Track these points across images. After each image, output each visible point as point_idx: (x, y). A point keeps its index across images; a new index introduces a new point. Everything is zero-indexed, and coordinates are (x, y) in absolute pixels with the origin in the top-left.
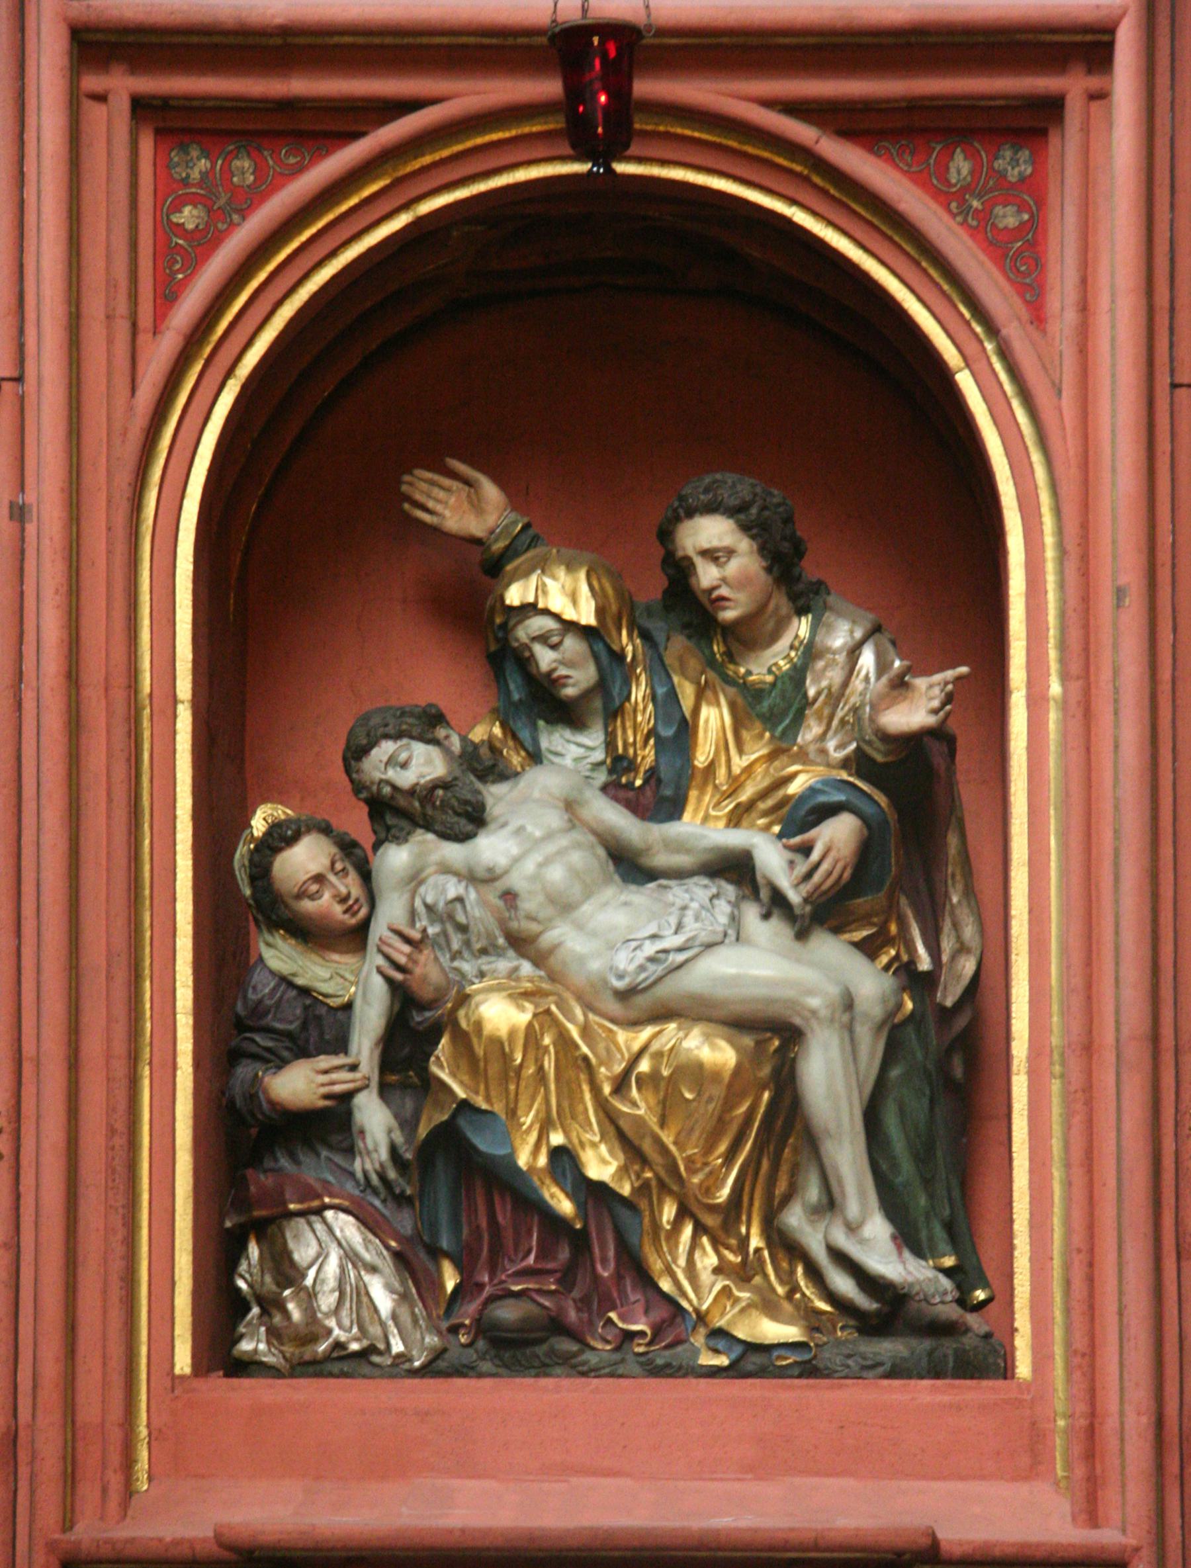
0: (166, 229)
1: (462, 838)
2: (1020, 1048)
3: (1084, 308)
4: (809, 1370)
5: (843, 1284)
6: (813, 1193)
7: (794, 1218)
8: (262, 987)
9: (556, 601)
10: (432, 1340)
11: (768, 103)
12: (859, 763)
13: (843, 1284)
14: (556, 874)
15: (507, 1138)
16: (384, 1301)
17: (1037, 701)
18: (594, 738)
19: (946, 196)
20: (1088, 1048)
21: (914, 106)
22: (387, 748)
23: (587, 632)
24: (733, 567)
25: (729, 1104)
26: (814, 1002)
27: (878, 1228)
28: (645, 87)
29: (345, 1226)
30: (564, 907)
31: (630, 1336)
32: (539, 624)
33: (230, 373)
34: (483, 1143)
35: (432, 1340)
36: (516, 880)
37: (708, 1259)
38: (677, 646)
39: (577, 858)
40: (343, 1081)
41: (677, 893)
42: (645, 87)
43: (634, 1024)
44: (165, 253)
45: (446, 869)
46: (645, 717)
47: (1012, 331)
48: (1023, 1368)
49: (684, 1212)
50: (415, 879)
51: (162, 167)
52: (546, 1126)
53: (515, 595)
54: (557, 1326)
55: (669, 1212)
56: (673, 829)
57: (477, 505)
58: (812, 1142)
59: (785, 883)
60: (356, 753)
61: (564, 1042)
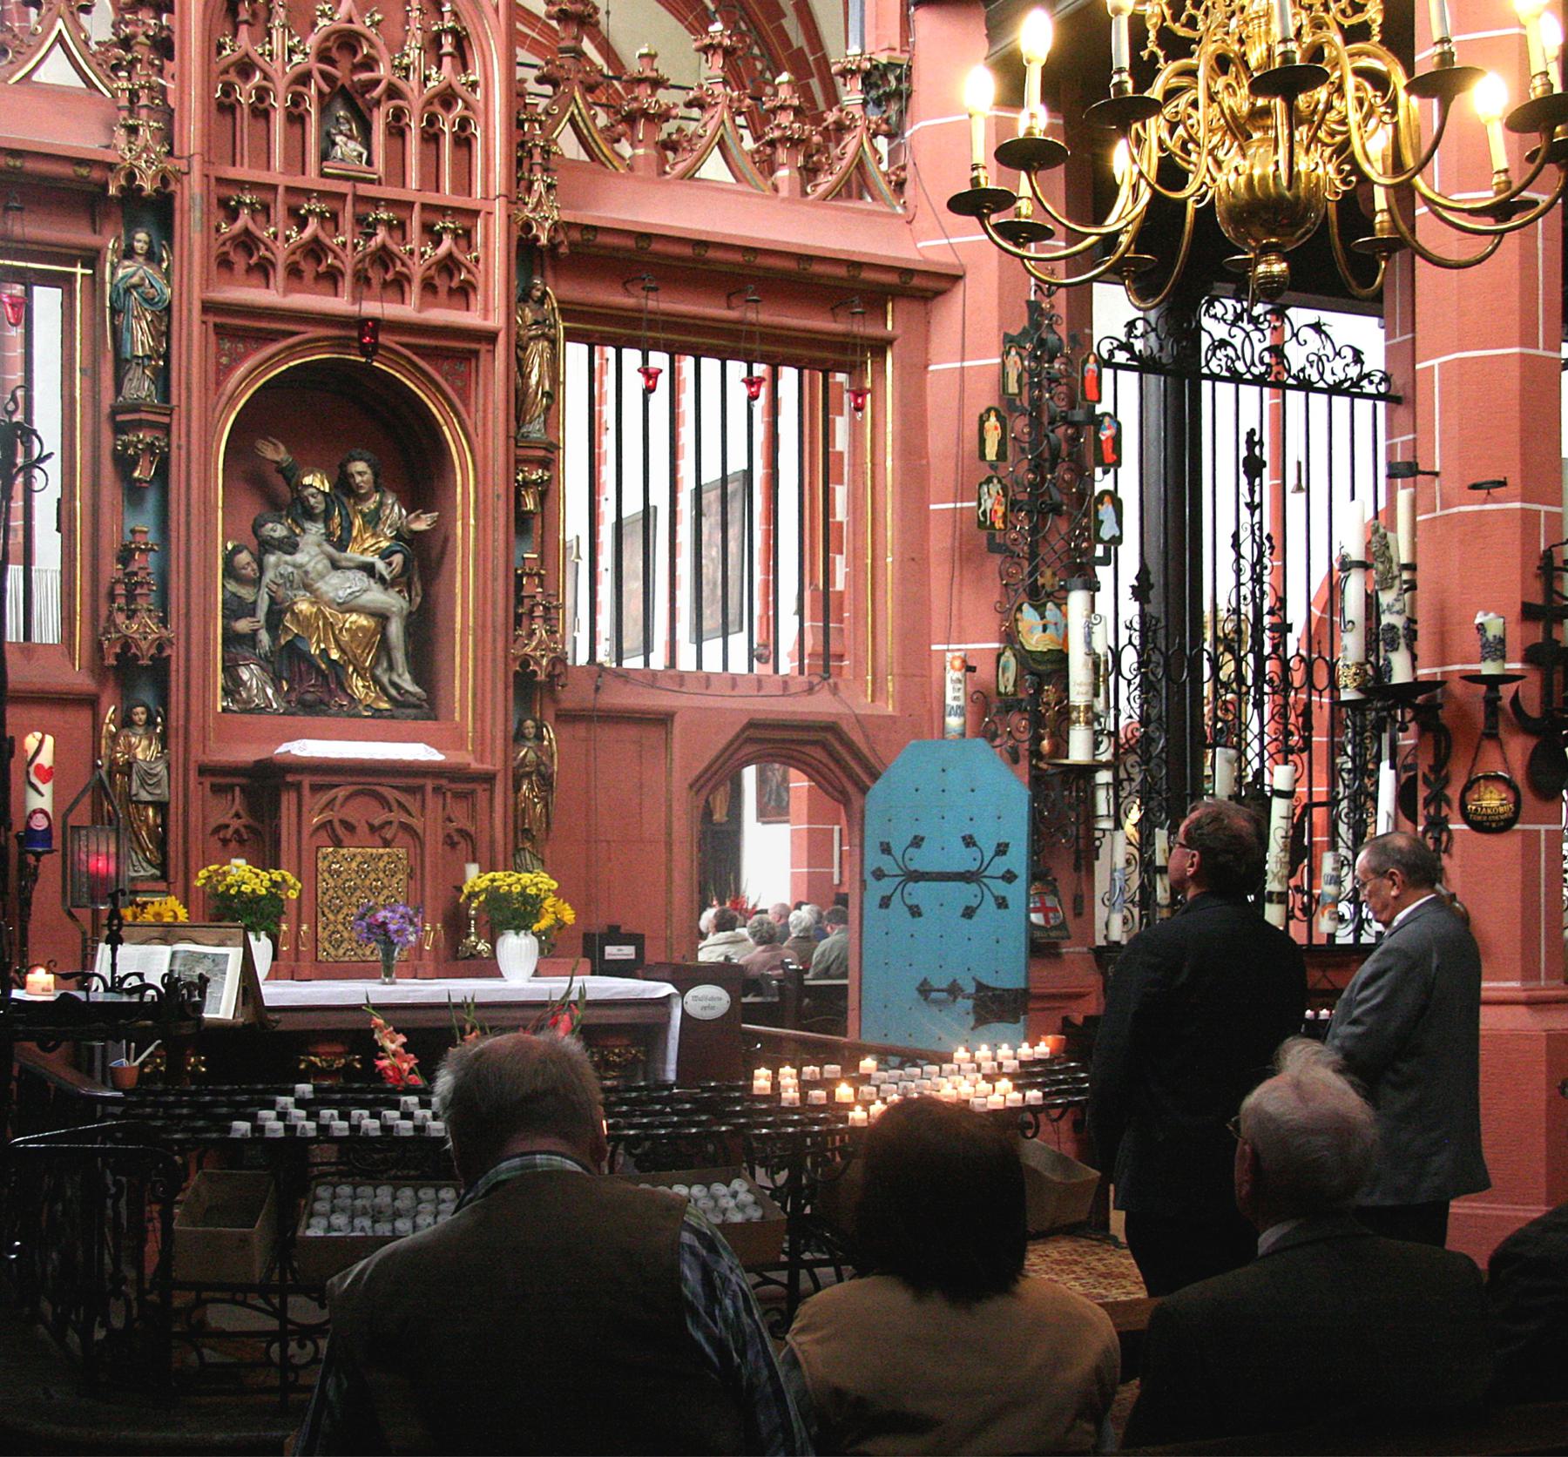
0: (218, 363)
1: (291, 554)
4: (393, 717)
5: (393, 692)
6: (385, 665)
7: (379, 672)
9: (317, 484)
12: (396, 538)
14: (320, 567)
15: (309, 646)
16: (270, 692)
19: (438, 370)
22: (270, 525)
24: (366, 477)
27: (407, 676)
28: (382, 339)
30: (322, 576)
32: (312, 490)
34: (300, 645)
36: (309, 568)
37: (360, 683)
40: (257, 626)
41: (350, 574)
44: (218, 371)
46: (337, 520)
47: (465, 416)
48: (457, 717)
49: (355, 670)
50: (277, 565)
51: (218, 344)
52: (318, 643)
54: (321, 702)
55: (351, 669)
59: (385, 573)
61: (325, 618)
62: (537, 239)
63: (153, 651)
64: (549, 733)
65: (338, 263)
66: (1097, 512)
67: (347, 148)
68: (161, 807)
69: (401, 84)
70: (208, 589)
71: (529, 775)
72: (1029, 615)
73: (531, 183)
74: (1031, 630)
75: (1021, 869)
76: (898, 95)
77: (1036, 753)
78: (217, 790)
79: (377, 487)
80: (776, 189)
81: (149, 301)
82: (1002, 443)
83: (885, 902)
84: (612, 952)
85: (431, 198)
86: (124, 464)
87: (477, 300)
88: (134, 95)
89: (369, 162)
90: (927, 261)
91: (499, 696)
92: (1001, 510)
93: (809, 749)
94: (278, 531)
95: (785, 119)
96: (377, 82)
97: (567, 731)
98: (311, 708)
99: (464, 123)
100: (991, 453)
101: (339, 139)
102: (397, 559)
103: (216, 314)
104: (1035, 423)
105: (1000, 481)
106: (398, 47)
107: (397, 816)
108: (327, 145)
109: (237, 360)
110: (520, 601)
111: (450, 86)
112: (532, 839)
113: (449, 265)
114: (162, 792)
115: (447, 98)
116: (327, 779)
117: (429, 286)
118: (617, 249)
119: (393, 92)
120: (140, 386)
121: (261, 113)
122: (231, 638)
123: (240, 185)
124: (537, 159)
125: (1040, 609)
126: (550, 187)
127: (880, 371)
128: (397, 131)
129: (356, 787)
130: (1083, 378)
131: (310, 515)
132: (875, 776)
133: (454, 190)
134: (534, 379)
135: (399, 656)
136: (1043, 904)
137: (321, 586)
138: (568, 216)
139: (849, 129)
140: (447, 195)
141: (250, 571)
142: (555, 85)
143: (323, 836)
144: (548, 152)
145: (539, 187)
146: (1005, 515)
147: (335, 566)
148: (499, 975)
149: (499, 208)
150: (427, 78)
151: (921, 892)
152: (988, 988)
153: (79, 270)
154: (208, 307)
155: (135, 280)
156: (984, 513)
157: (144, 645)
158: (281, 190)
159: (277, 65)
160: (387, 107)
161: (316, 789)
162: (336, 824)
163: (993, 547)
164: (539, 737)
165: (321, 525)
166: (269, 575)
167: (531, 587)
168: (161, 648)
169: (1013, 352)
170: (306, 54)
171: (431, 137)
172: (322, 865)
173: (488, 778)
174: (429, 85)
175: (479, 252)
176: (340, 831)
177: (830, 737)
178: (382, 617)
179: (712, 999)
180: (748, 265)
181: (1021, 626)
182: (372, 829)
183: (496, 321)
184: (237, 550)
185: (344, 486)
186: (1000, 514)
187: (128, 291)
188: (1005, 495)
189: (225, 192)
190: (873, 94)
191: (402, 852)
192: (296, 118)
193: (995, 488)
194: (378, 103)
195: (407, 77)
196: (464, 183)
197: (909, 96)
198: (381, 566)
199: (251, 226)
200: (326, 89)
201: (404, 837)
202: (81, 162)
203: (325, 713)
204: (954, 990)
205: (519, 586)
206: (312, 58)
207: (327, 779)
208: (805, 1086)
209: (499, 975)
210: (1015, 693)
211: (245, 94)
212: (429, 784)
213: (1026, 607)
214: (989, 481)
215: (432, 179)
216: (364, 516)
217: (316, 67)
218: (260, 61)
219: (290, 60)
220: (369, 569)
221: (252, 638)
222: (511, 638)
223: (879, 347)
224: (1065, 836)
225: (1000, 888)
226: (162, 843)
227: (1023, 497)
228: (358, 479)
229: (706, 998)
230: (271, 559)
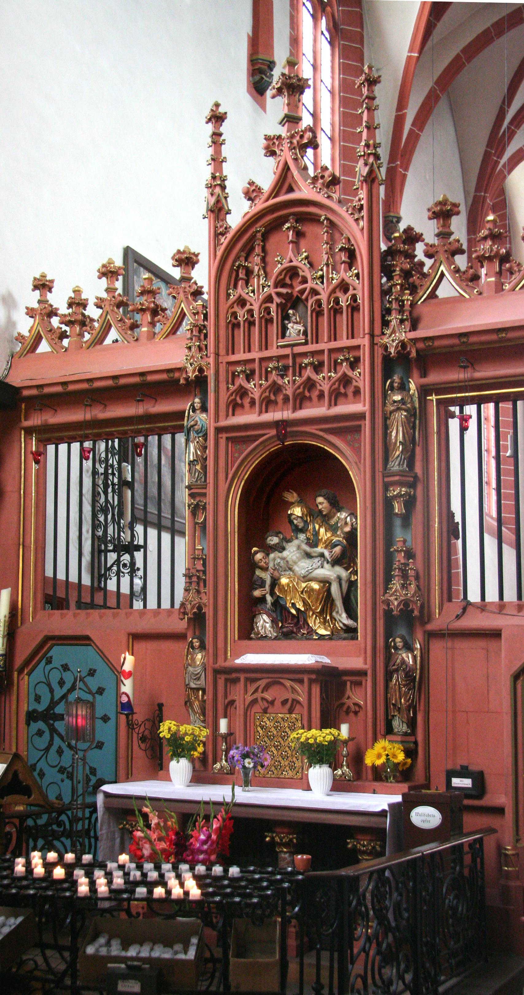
1: (281, 552)
4: (331, 639)
8: (255, 578)
10: (275, 634)
11: (317, 430)
14: (294, 558)
21: (340, 428)
22: (270, 538)
23: (300, 517)
24: (324, 505)
25: (318, 595)
26: (332, 578)
27: (344, 615)
28: (289, 429)
29: (265, 617)
30: (295, 563)
31: (304, 634)
33: (243, 479)
35: (275, 634)
36: (288, 559)
39: (298, 555)
40: (264, 593)
42: (289, 429)
43: (306, 582)
45: (279, 557)
50: (274, 559)
54: (292, 632)
55: (311, 613)
56: (315, 549)
57: (293, 497)
58: (333, 600)
62: (409, 353)
84: (467, 783)
98: (287, 635)
101: (289, 326)
103: (226, 433)
114: (202, 682)
116: (254, 675)
118: (452, 346)
129: (270, 680)
147: (309, 556)
148: (309, 789)
170: (269, 286)
173: (362, 673)
174: (333, 282)
178: (326, 583)
179: (429, 815)
180: (502, 340)
195: (322, 283)
198: (327, 553)
203: (295, 638)
206: (271, 287)
207: (254, 675)
208: (49, 866)
209: (309, 789)
211: (242, 315)
217: (273, 291)
218: (246, 297)
219: (263, 290)
221: (263, 599)
228: (320, 507)
229: (423, 815)
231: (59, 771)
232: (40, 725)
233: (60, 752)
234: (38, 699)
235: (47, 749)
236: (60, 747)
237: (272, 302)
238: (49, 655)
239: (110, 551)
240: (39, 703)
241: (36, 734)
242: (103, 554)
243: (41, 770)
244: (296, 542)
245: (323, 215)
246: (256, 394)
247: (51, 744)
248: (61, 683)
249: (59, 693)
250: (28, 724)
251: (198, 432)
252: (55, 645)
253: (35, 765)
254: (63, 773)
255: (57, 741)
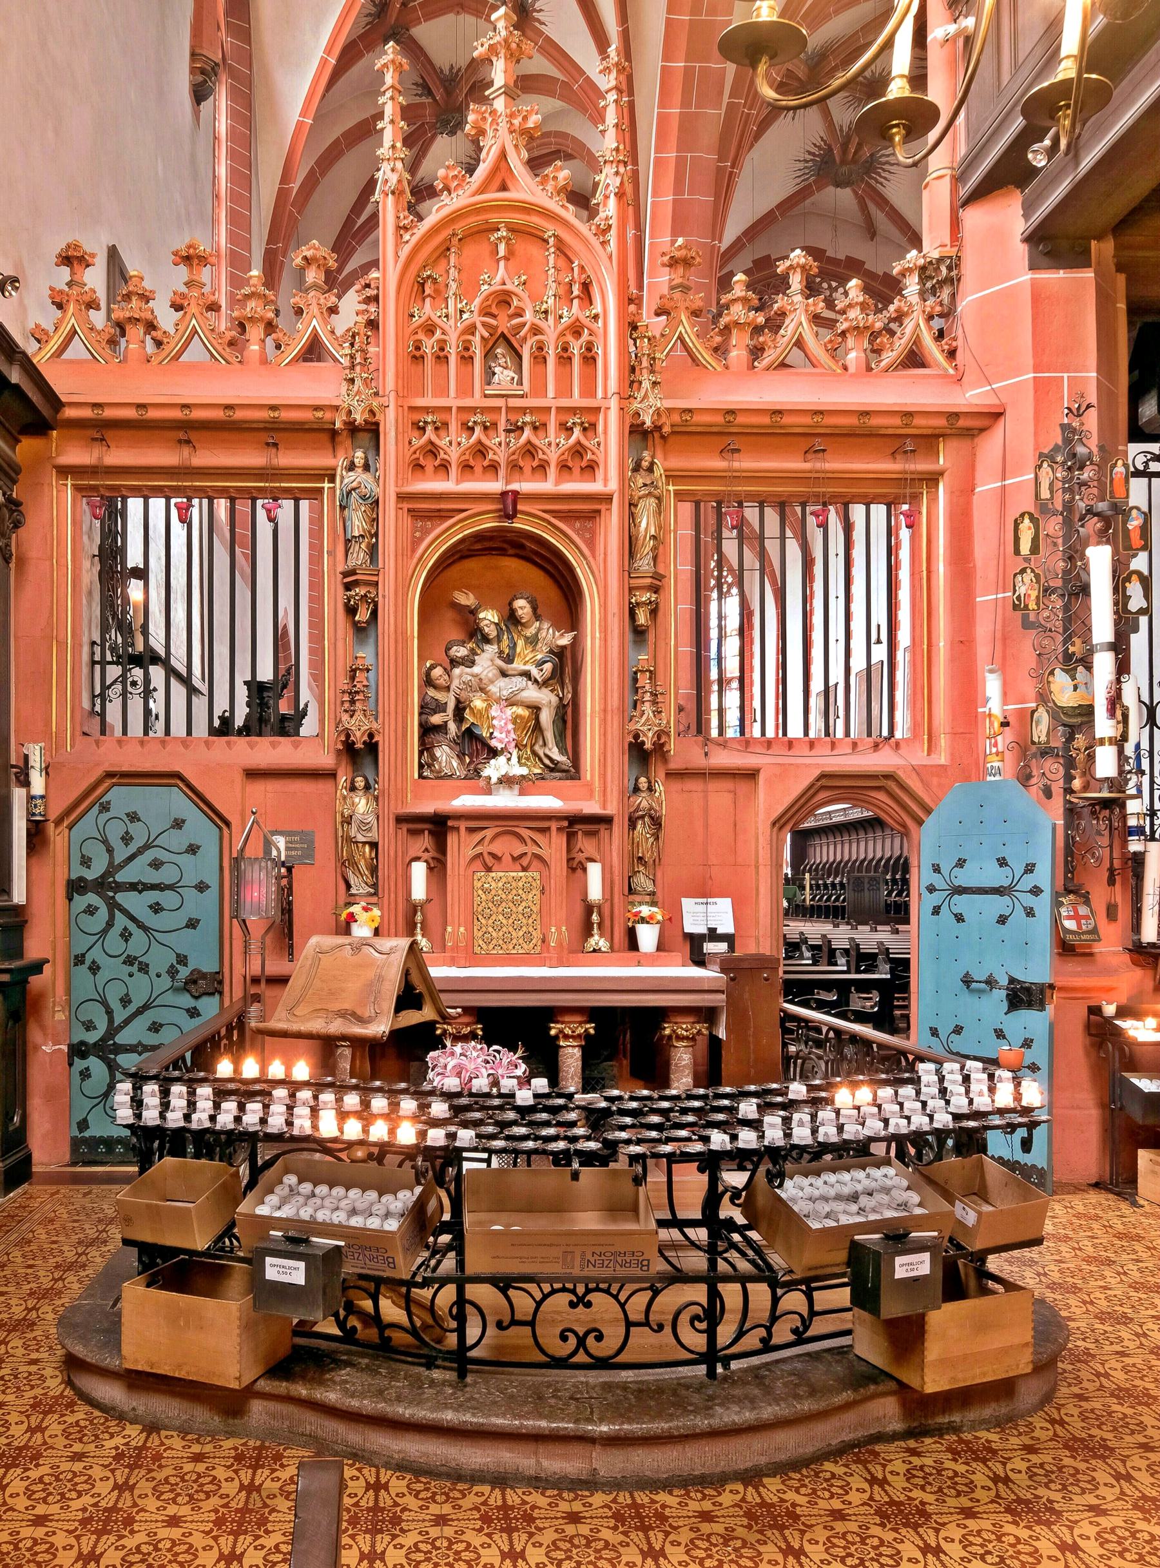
2: (589, 711)
3: (605, 554)
5: (547, 762)
7: (537, 748)
9: (490, 617)
12: (551, 652)
13: (547, 762)
16: (455, 764)
17: (593, 638)
18: (495, 647)
20: (605, 711)
27: (555, 749)
30: (492, 682)
38: (512, 628)
47: (590, 559)
50: (461, 676)
53: (481, 616)
60: (448, 649)
63: (366, 738)
64: (659, 787)
65: (496, 458)
66: (1125, 588)
67: (504, 376)
68: (374, 845)
69: (542, 324)
70: (406, 693)
71: (642, 817)
72: (1061, 679)
73: (640, 383)
74: (1062, 690)
75: (1045, 884)
76: (949, 281)
77: (1069, 791)
78: (413, 833)
79: (537, 617)
80: (845, 368)
81: (364, 498)
82: (1035, 541)
83: (936, 911)
85: (565, 402)
86: (351, 611)
87: (600, 474)
88: (352, 357)
89: (520, 383)
90: (971, 405)
91: (618, 760)
92: (1034, 594)
93: (873, 794)
94: (460, 652)
95: (854, 313)
96: (524, 325)
97: (676, 786)
99: (589, 347)
100: (1025, 548)
101: (497, 370)
102: (548, 667)
104: (1068, 523)
105: (1033, 571)
106: (536, 298)
107: (532, 849)
108: (489, 374)
109: (426, 532)
110: (636, 690)
111: (577, 320)
112: (645, 864)
113: (578, 451)
114: (373, 836)
115: (576, 330)
117: (564, 467)
119: (536, 330)
120: (358, 556)
121: (441, 358)
122: (427, 730)
123: (427, 410)
124: (645, 363)
125: (1071, 673)
126: (655, 383)
127: (934, 499)
128: (540, 358)
130: (1112, 480)
131: (486, 640)
132: (928, 811)
133: (582, 395)
134: (643, 525)
135: (549, 735)
136: (1076, 911)
137: (493, 689)
138: (669, 404)
139: (906, 314)
140: (576, 399)
141: (442, 682)
142: (667, 313)
143: (478, 864)
144: (654, 359)
145: (646, 385)
146: (1038, 597)
147: (504, 674)
149: (614, 403)
150: (561, 317)
151: (962, 903)
152: (1019, 982)
153: (326, 485)
154: (401, 497)
155: (354, 484)
156: (1019, 598)
157: (358, 734)
158: (454, 410)
159: (452, 322)
160: (532, 341)
161: (471, 830)
162: (486, 855)
163: (1027, 625)
164: (650, 789)
165: (495, 647)
166: (455, 683)
167: (644, 681)
168: (371, 736)
169: (1045, 465)
171: (565, 359)
172: (478, 884)
173: (607, 820)
175: (601, 438)
176: (489, 861)
177: (891, 785)
178: (536, 709)
181: (1053, 687)
182: (515, 859)
183: (613, 486)
184: (432, 667)
185: (512, 619)
186: (1033, 597)
187: (349, 493)
188: (1038, 582)
189: (416, 417)
190: (929, 285)
191: (536, 875)
192: (466, 359)
193: (1029, 576)
194: (525, 339)
196: (589, 389)
197: (959, 280)
198: (535, 672)
199: (434, 438)
200: (486, 334)
201: (535, 863)
202: (317, 408)
204: (991, 982)
205: (635, 680)
206: (476, 313)
210: (1048, 742)
211: (429, 346)
212: (554, 826)
213: (1057, 671)
214: (1023, 571)
215: (564, 389)
216: (527, 638)
217: (478, 320)
218: (438, 321)
220: (527, 675)
222: (627, 719)
223: (933, 479)
224: (1093, 856)
225: (1029, 900)
226: (374, 870)
227: (1058, 583)
230: (457, 671)
231: (124, 963)
232: (92, 898)
233: (126, 935)
234: (86, 862)
235: (105, 932)
236: (125, 929)
237: (473, 334)
238: (103, 800)
239: (110, 663)
240: (89, 867)
241: (84, 912)
242: (98, 667)
243: (94, 962)
244: (485, 656)
245: (550, 230)
246: (454, 455)
247: (110, 924)
248: (127, 839)
249: (121, 854)
250: (70, 899)
251: (364, 498)
252: (114, 785)
253: (83, 955)
254: (132, 964)
255: (121, 920)
